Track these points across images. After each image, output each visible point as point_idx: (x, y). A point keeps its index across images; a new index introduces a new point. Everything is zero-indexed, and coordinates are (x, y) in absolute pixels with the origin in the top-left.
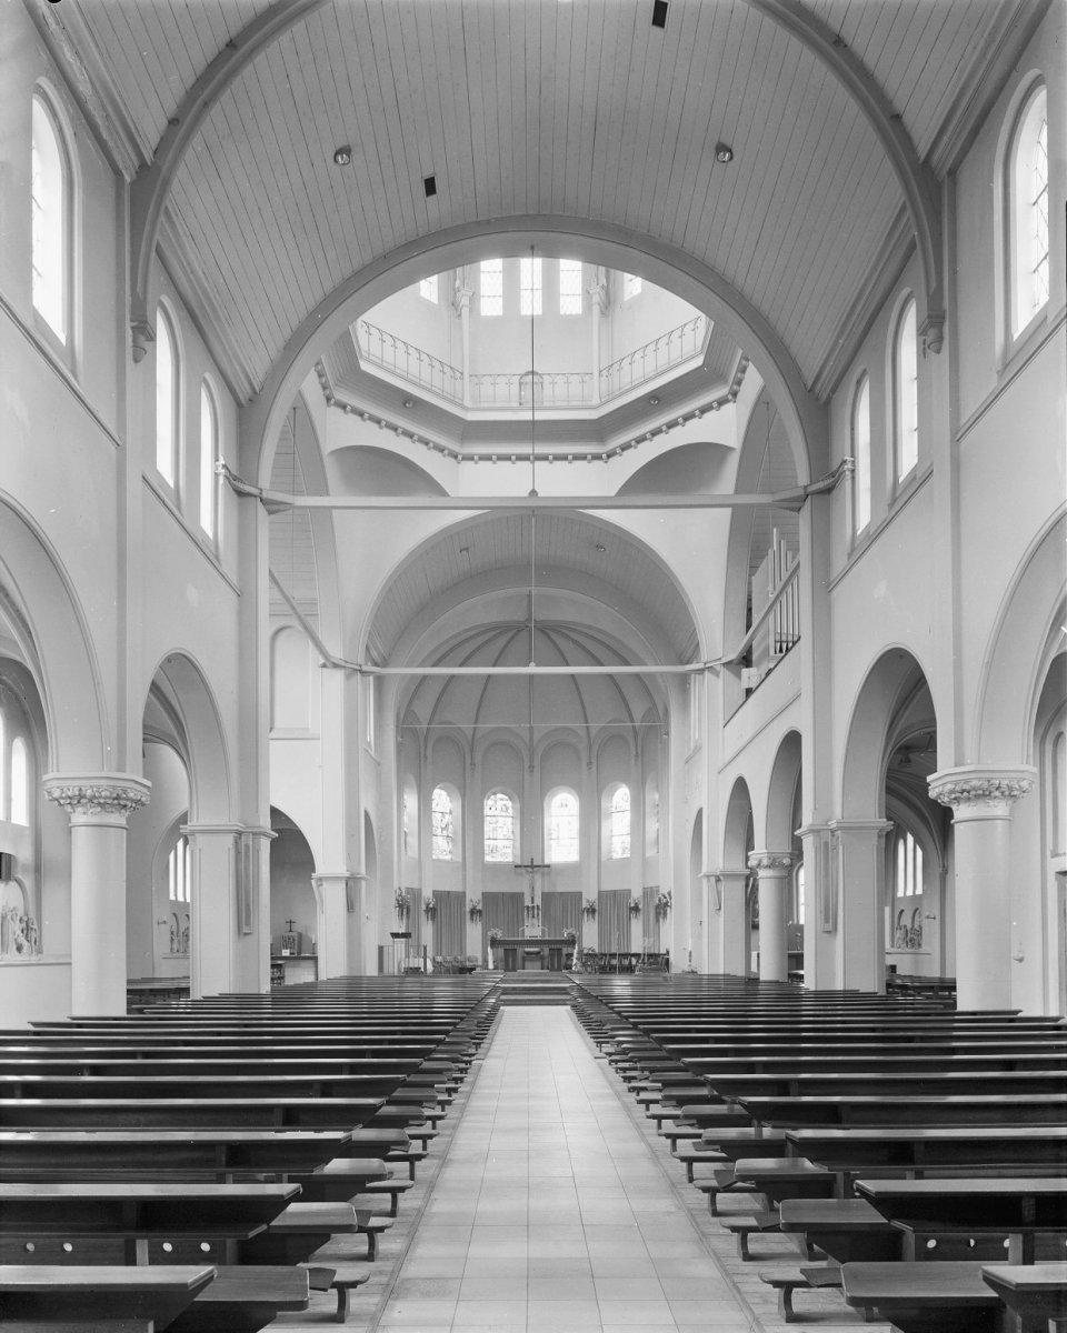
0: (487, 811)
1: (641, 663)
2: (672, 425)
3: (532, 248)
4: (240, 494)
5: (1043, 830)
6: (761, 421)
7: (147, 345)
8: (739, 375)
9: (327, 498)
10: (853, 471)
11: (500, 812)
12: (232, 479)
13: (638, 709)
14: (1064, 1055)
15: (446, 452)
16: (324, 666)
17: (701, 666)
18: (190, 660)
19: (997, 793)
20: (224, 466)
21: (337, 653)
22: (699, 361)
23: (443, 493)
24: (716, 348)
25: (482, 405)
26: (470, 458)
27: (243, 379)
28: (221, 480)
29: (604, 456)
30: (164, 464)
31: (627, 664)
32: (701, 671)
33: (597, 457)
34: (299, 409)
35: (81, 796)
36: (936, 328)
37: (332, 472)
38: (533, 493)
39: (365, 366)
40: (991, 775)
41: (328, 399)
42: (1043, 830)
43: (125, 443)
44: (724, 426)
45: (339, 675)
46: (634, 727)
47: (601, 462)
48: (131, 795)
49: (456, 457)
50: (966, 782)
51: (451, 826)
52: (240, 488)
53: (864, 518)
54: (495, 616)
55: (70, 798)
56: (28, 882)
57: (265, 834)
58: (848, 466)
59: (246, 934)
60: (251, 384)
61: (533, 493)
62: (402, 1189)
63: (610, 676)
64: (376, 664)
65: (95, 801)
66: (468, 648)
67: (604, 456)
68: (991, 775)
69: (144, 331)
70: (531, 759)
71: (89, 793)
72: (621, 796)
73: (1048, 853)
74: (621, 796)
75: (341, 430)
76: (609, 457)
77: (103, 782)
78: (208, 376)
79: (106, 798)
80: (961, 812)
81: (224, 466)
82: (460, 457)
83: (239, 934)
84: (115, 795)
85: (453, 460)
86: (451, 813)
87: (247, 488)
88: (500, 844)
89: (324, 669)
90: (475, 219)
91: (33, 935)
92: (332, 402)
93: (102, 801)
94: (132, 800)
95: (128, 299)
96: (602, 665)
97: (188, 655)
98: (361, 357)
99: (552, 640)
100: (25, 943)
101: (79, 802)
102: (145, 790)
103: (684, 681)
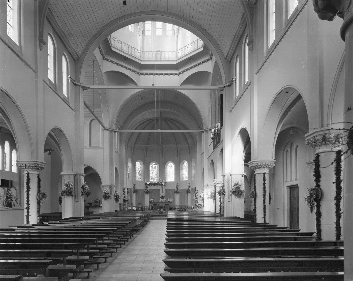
0: (150, 168)
1: (190, 129)
2: (195, 66)
3: (153, 19)
4: (75, 85)
5: (283, 175)
6: (216, 67)
7: (44, 46)
9: (104, 86)
10: (236, 80)
11: (154, 167)
12: (72, 81)
13: (190, 141)
15: (136, 72)
16: (104, 130)
17: (203, 130)
18: (61, 130)
19: (265, 167)
20: (70, 77)
21: (107, 126)
22: (202, 49)
23: (136, 85)
24: (205, 46)
25: (146, 60)
26: (142, 74)
27: (75, 53)
28: (69, 81)
29: (178, 74)
30: (51, 76)
31: (187, 129)
32: (203, 132)
33: (176, 74)
34: (95, 61)
35: (26, 166)
36: (251, 44)
37: (105, 77)
38: (153, 85)
39: (113, 49)
40: (263, 162)
41: (103, 58)
42: (283, 175)
43: (37, 71)
44: (208, 67)
45: (108, 133)
46: (189, 146)
47: (177, 75)
48: (40, 166)
49: (139, 74)
50: (258, 163)
51: (141, 172)
52: (74, 83)
53: (238, 94)
54: (151, 116)
55: (23, 166)
56: (17, 187)
57: (83, 175)
58: (235, 79)
59: (77, 202)
60: (78, 56)
61: (153, 85)
62: (91, 272)
63: (183, 133)
64: (120, 129)
65: (30, 167)
66: (136, 126)
67: (178, 74)
68: (263, 162)
69: (43, 43)
70: (162, 154)
71: (28, 165)
72: (185, 164)
73: (285, 181)
74: (185, 164)
75: (108, 67)
76: (179, 74)
77: (32, 162)
78: (65, 53)
79: (33, 166)
81: (70, 77)
82: (140, 74)
83: (75, 201)
84: (35, 166)
85: (138, 74)
86: (141, 168)
87: (77, 83)
88: (154, 176)
89: (104, 131)
90: (137, 11)
91: (18, 202)
92: (105, 59)
93: (32, 167)
94: (40, 167)
95: (38, 33)
96: (180, 130)
97: (58, 128)
98: (112, 46)
99: (167, 123)
100: (16, 204)
101: (25, 167)
102: (44, 165)
103: (200, 134)
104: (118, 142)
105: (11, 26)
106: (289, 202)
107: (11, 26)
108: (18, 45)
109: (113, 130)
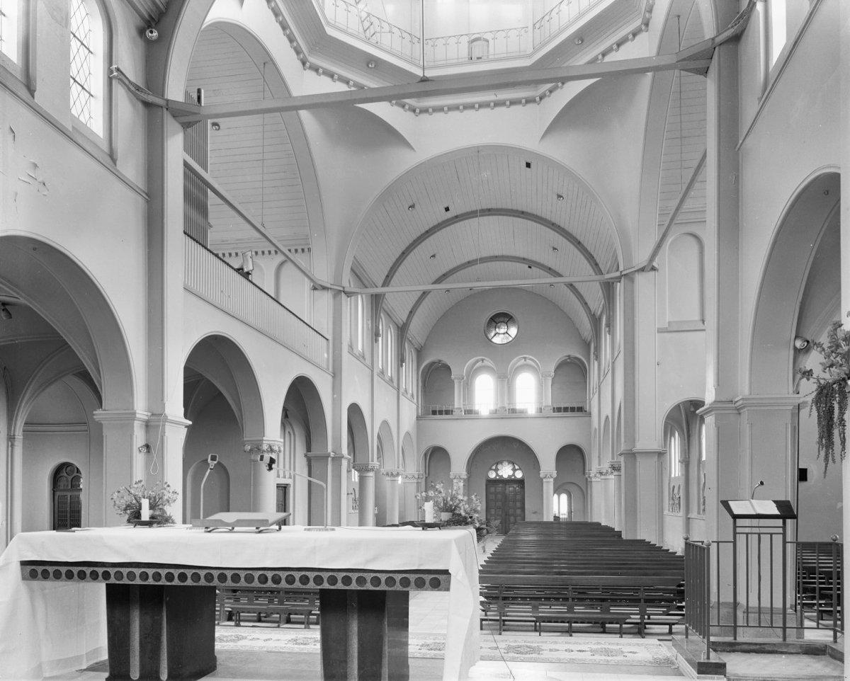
8: (647, 15)
14: (164, 676)
16: (315, 289)
21: (324, 277)
33: (529, 101)
39: (330, 31)
41: (304, 64)
49: (414, 111)
76: (541, 99)
80: (544, 480)
82: (418, 111)
89: (316, 292)
92: (308, 65)
104: (393, 341)
105: (88, 49)
106: (106, 48)
107: (88, 49)
108: (779, 513)
109: (342, 289)
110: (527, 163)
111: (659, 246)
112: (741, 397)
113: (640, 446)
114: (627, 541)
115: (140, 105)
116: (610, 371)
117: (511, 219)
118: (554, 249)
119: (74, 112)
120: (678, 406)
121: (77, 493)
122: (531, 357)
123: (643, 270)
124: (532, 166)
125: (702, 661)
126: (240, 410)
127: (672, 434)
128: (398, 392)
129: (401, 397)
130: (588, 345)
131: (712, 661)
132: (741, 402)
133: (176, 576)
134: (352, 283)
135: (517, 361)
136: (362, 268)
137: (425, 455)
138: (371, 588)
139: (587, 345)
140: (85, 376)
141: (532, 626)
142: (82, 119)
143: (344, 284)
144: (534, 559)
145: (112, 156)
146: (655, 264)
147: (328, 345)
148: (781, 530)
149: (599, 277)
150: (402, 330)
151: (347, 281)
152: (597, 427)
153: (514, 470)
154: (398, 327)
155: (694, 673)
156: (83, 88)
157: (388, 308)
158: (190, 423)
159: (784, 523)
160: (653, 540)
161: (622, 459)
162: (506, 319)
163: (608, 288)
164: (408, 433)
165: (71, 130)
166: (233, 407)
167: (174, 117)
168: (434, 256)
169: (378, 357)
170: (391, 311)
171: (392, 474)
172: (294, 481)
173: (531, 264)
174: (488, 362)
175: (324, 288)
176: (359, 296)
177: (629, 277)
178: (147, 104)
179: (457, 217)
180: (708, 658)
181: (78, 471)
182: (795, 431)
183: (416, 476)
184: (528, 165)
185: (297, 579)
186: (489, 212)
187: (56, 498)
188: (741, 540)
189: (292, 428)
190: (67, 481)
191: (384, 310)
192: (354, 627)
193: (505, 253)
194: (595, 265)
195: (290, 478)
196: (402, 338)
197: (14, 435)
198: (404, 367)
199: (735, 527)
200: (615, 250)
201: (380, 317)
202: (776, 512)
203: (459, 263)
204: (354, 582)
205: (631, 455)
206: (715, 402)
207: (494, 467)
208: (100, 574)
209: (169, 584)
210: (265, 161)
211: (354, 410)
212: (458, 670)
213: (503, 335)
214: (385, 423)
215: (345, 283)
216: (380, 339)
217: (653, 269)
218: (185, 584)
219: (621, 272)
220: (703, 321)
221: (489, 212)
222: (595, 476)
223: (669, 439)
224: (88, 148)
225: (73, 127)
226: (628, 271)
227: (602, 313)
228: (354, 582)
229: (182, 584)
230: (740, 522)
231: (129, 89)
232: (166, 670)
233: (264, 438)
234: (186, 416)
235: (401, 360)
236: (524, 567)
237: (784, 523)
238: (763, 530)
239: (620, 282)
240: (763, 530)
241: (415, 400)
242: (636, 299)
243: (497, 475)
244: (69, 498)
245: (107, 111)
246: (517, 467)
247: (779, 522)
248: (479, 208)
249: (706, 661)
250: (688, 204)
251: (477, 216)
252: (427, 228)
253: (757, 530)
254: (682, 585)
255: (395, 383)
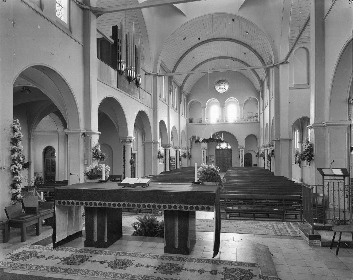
16: (146, 74)
109: (157, 74)
110: (234, 21)
111: (290, 53)
112: (325, 122)
113: (281, 138)
114: (276, 177)
115: (80, 10)
116: (269, 104)
117: (226, 42)
118: (244, 53)
119: (56, 15)
120: (298, 120)
121: (53, 158)
122: (234, 98)
123: (283, 63)
124: (235, 20)
125: (310, 234)
126: (118, 126)
127: (295, 130)
128: (179, 114)
129: (180, 116)
130: (259, 93)
131: (315, 234)
132: (325, 124)
133: (112, 204)
134: (160, 71)
135: (229, 99)
136: (164, 64)
137: (190, 139)
138: (185, 210)
139: (258, 93)
140: (59, 114)
141: (238, 214)
142: (59, 17)
143: (157, 72)
144: (238, 186)
145: (70, 30)
146: (288, 61)
147: (151, 97)
148: (343, 181)
149: (264, 67)
150: (180, 89)
151: (159, 71)
152: (263, 127)
153: (227, 145)
154: (179, 87)
155: (307, 239)
156: (60, 5)
157: (175, 80)
158: (101, 133)
159: (344, 178)
160: (288, 177)
161: (274, 142)
162: (224, 82)
163: (268, 71)
164: (183, 131)
165: (56, 22)
166: (115, 124)
167: (93, 13)
168: (193, 58)
169: (171, 102)
170: (176, 81)
171: (177, 148)
172: (138, 151)
173: (234, 59)
174: (216, 100)
175: (150, 74)
176: (163, 77)
177: (277, 66)
178: (83, 9)
179: (203, 42)
180: (313, 233)
181: (54, 150)
182: (349, 136)
183: (187, 148)
184: (233, 20)
185: (157, 206)
186: (217, 39)
187: (46, 160)
188: (326, 184)
189: (137, 131)
190: (50, 153)
191: (174, 81)
192: (177, 224)
193: (223, 55)
194: (262, 60)
195: (136, 150)
196: (181, 91)
197: (31, 137)
198: (181, 104)
199: (323, 179)
200: (271, 55)
201: (172, 84)
202: (341, 173)
203: (204, 60)
204: (178, 208)
205: (278, 141)
206: (314, 123)
207: (219, 144)
208: (84, 203)
209: (109, 207)
210: (126, 24)
211: (162, 122)
212: (38, 70)
213: (223, 88)
214: (174, 128)
215: (158, 72)
216: (172, 93)
217: (287, 63)
218: (115, 207)
219: (273, 64)
220: (309, 84)
221: (217, 39)
222: (262, 148)
223: (294, 132)
224: (62, 29)
225: (57, 21)
226: (276, 64)
227: (265, 79)
228: (178, 208)
229: (114, 207)
230: (325, 177)
231: (76, 3)
232: (107, 238)
233: (128, 137)
234: (99, 130)
235: (180, 101)
236: (234, 190)
237: (344, 178)
238: (335, 181)
239: (273, 68)
240: (335, 181)
241: (186, 117)
242: (280, 75)
243: (220, 147)
244: (51, 160)
245: (68, 14)
246: (228, 144)
247: (342, 178)
248: (213, 38)
249: (312, 234)
250: (303, 35)
251: (212, 41)
252: (191, 47)
253: (333, 181)
254: (301, 198)
255: (178, 110)
